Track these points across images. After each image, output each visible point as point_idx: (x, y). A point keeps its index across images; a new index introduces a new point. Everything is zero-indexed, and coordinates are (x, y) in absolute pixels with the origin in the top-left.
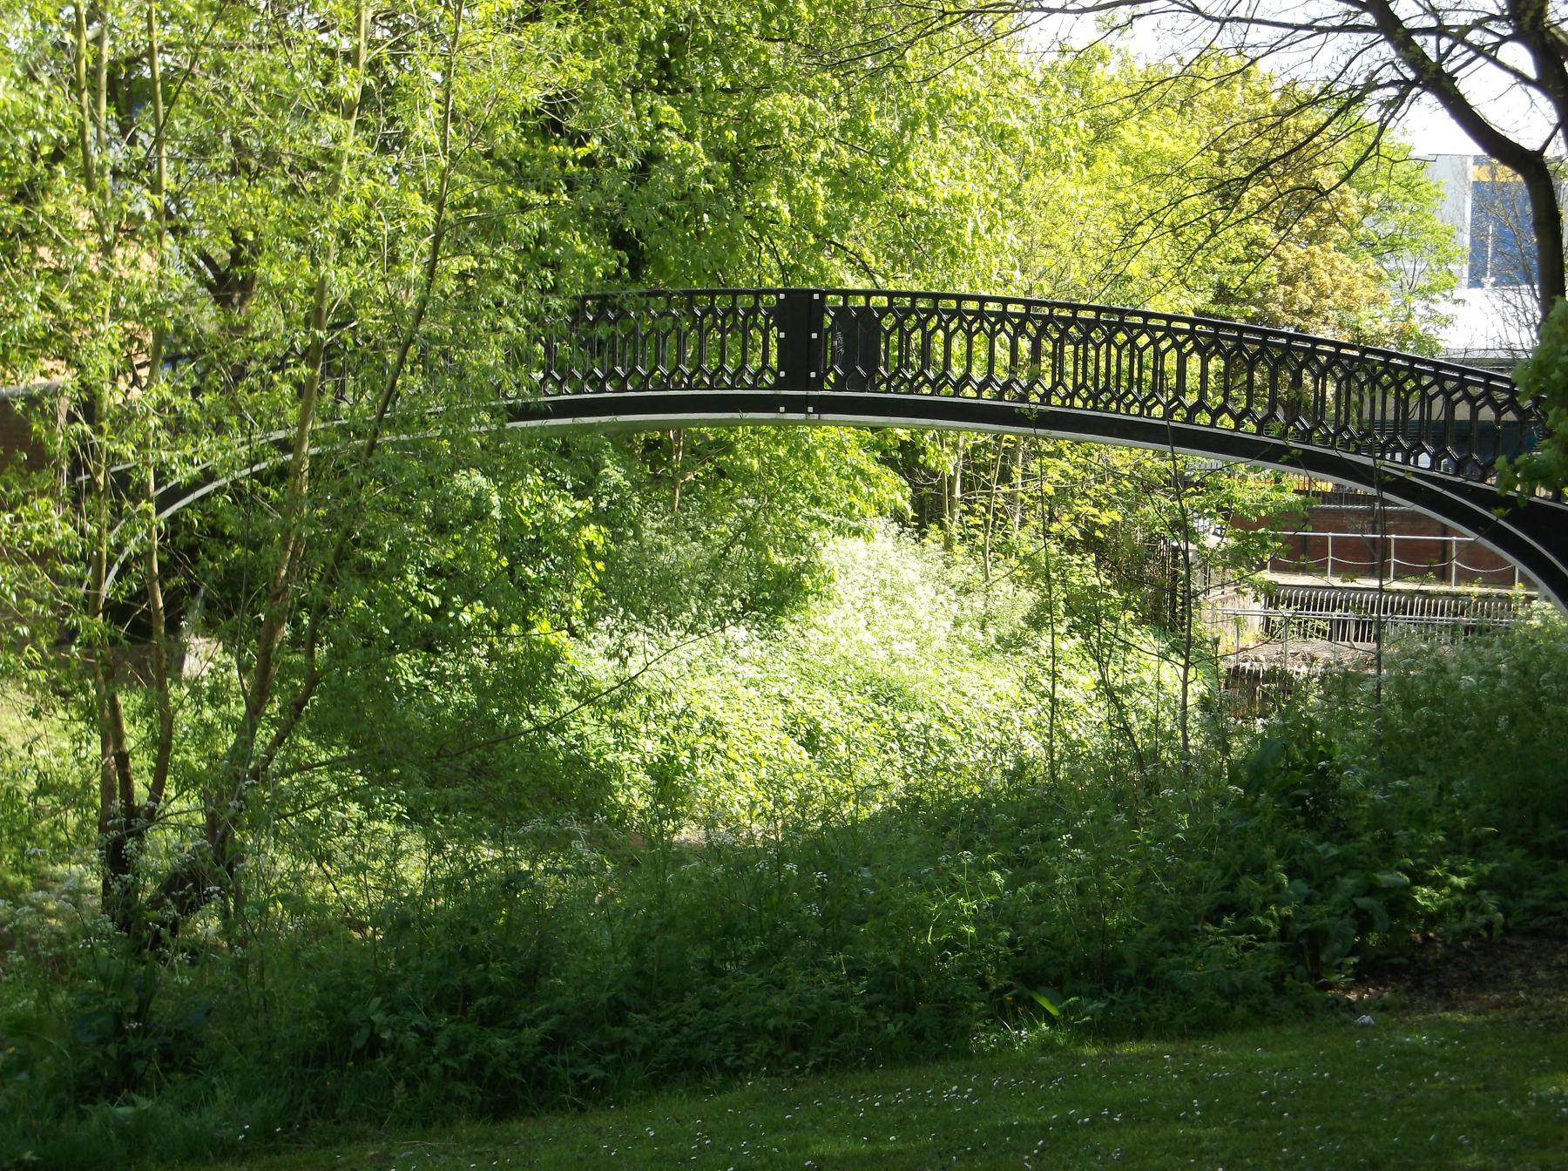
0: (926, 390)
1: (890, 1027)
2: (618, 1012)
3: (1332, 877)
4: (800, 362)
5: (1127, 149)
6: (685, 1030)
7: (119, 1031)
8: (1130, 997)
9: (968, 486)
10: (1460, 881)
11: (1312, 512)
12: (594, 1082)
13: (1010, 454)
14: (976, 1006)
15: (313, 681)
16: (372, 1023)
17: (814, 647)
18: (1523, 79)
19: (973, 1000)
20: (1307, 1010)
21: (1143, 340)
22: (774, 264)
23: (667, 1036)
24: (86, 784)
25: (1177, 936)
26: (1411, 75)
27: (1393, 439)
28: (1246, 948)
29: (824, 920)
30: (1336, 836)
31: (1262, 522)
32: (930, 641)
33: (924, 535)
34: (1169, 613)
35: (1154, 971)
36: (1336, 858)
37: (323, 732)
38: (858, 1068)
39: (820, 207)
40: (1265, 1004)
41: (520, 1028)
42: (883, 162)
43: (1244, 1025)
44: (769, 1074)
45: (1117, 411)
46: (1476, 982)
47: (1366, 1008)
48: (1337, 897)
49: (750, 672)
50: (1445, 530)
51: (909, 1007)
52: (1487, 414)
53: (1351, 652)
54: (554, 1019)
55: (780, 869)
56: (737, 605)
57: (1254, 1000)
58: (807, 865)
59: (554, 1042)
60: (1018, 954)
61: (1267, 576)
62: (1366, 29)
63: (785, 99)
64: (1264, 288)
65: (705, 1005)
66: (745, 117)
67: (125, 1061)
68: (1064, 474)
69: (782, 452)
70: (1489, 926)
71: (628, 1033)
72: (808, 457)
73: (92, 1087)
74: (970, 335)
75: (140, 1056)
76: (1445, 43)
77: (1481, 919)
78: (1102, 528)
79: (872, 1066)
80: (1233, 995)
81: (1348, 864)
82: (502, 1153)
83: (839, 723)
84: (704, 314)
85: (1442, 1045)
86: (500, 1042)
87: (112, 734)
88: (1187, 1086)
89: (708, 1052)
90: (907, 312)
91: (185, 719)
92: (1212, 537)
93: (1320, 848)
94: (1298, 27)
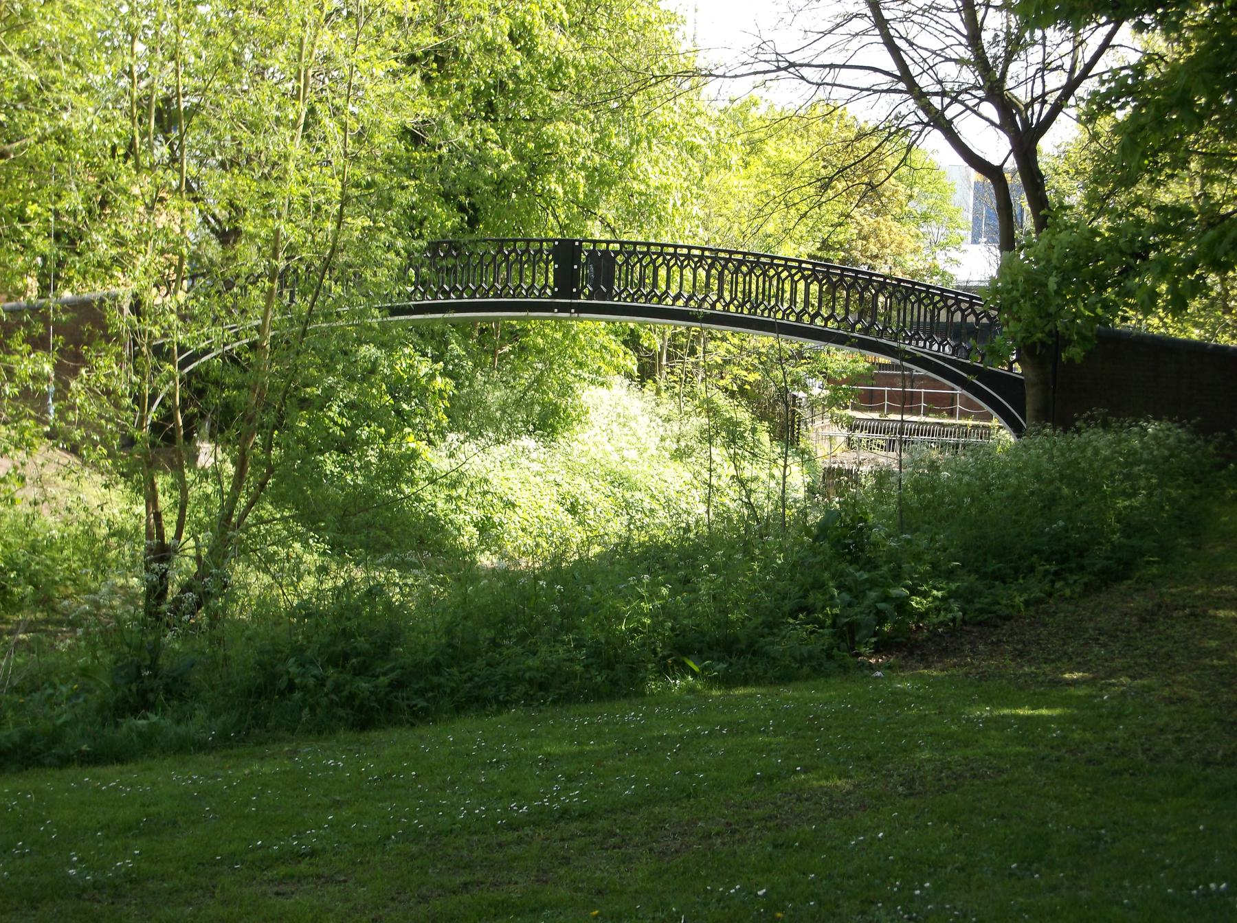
1: (599, 678)
2: (437, 667)
3: (864, 591)
4: (566, 283)
5: (769, 158)
7: (139, 675)
8: (742, 661)
9: (670, 357)
10: (939, 594)
12: (422, 709)
13: (697, 338)
15: (271, 470)
16: (288, 673)
18: (992, 123)
19: (650, 661)
20: (844, 669)
21: (772, 272)
22: (555, 223)
23: (466, 682)
24: (137, 528)
25: (772, 626)
26: (926, 120)
27: (917, 333)
28: (812, 632)
29: (563, 614)
30: (868, 567)
31: (844, 381)
32: (646, 449)
33: (644, 386)
34: (787, 434)
35: (757, 646)
36: (867, 580)
37: (278, 502)
38: (578, 702)
39: (581, 190)
40: (821, 665)
41: (378, 677)
42: (620, 163)
43: (807, 678)
44: (524, 705)
46: (944, 652)
47: (878, 667)
48: (867, 603)
49: (536, 467)
50: (953, 389)
51: (610, 666)
53: (888, 459)
55: (536, 583)
56: (531, 428)
57: (814, 663)
58: (551, 584)
59: (397, 685)
60: (677, 635)
61: (849, 412)
62: (900, 92)
63: (561, 125)
64: (849, 242)
65: (489, 664)
66: (537, 137)
67: (142, 694)
68: (728, 351)
69: (558, 335)
70: (954, 620)
71: (442, 680)
72: (574, 338)
74: (682, 268)
75: (152, 690)
76: (947, 100)
77: (950, 616)
78: (750, 384)
79: (586, 701)
80: (802, 661)
81: (873, 584)
82: (363, 749)
83: (590, 498)
84: (510, 253)
85: (918, 689)
86: (364, 685)
87: (152, 500)
88: (768, 713)
89: (489, 692)
90: (631, 254)
91: (194, 492)
92: (817, 389)
93: (857, 574)
94: (862, 90)
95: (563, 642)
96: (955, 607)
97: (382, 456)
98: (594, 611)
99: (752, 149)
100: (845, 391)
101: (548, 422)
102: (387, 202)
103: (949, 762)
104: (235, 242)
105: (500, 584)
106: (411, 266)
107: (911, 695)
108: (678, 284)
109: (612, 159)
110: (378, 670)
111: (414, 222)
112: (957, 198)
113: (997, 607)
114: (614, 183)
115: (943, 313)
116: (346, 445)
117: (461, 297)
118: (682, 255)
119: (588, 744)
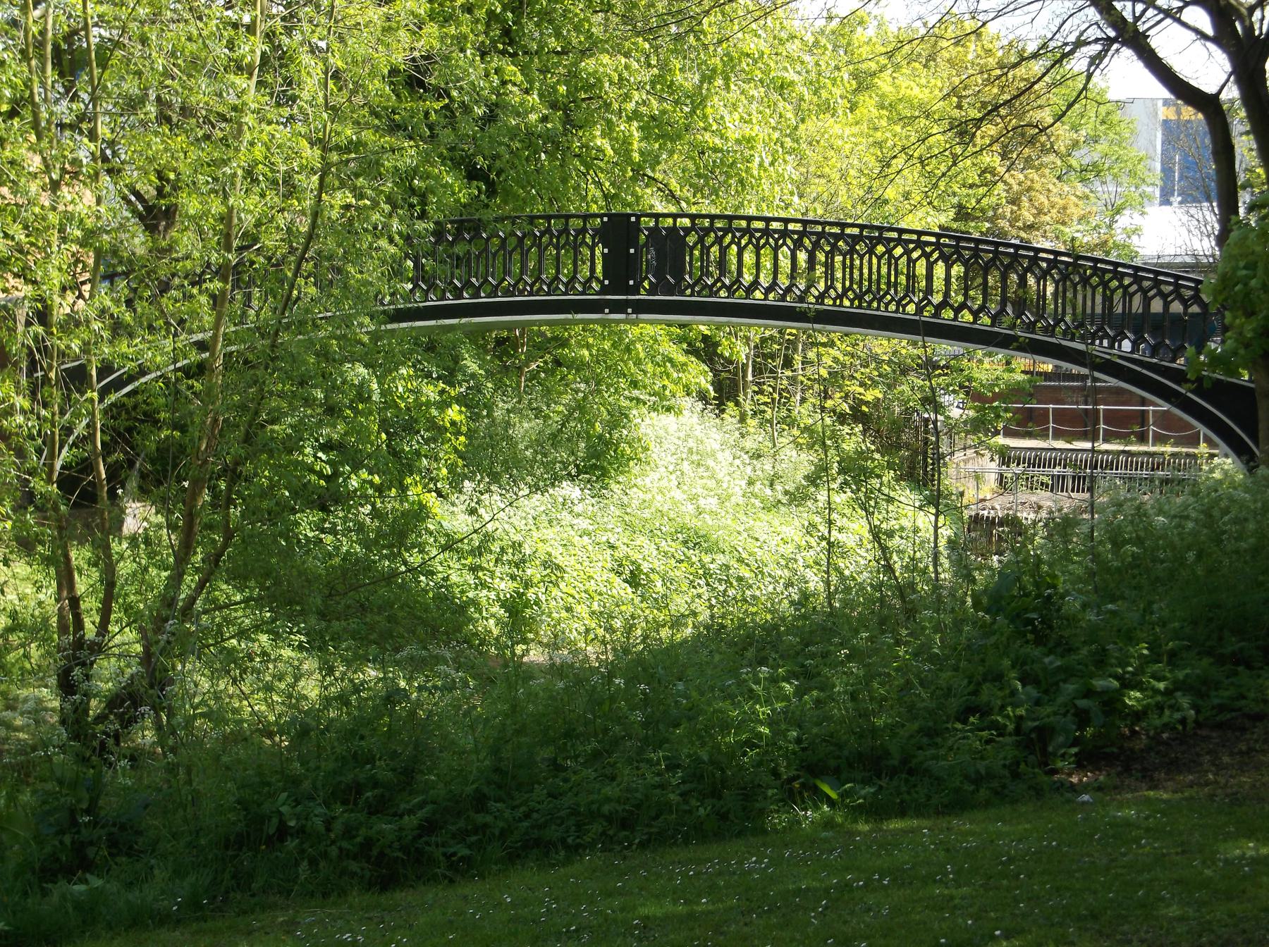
0: (723, 293)
1: (701, 810)
2: (480, 801)
3: (1057, 684)
4: (621, 272)
5: (883, 96)
6: (535, 815)
7: (74, 823)
9: (758, 371)
11: (1036, 388)
12: (462, 859)
13: (792, 344)
14: (770, 792)
15: (228, 536)
16: (281, 814)
17: (635, 503)
21: (898, 251)
23: (520, 820)
25: (932, 733)
27: (1101, 329)
28: (988, 742)
29: (645, 725)
30: (1059, 650)
31: (996, 397)
33: (723, 411)
34: (921, 471)
35: (915, 761)
36: (1059, 668)
37: (239, 578)
38: (675, 843)
39: (635, 146)
41: (401, 816)
43: (987, 804)
45: (878, 309)
46: (1174, 766)
47: (1084, 788)
48: (1060, 700)
49: (584, 524)
50: (1144, 402)
51: (716, 794)
52: (1176, 307)
53: (1070, 501)
54: (428, 808)
57: (995, 784)
58: (631, 681)
59: (429, 827)
60: (803, 749)
61: (1001, 440)
63: (605, 59)
65: (550, 795)
66: (572, 75)
67: (79, 848)
68: (836, 360)
69: (607, 345)
70: (1183, 721)
72: (628, 350)
73: (51, 871)
74: (758, 249)
77: (1177, 716)
78: (867, 403)
79: (686, 842)
80: (978, 780)
81: (1068, 673)
83: (656, 564)
85: (1147, 818)
86: (385, 827)
87: (66, 579)
89: (553, 833)
90: (707, 231)
92: (956, 409)
93: (1047, 660)
95: (649, 761)
96: (1185, 702)
97: (375, 514)
98: (690, 719)
99: (860, 84)
100: (990, 409)
101: (599, 461)
102: (371, 168)
103: (1209, 922)
104: (167, 228)
105: (561, 685)
106: (407, 256)
107: (1138, 827)
108: (759, 269)
109: (677, 102)
110: (403, 806)
111: (411, 197)
112: (1142, 141)
113: (1243, 702)
114: (679, 137)
115: (1137, 300)
116: (328, 498)
117: (477, 296)
118: (757, 230)
119: (699, 903)
